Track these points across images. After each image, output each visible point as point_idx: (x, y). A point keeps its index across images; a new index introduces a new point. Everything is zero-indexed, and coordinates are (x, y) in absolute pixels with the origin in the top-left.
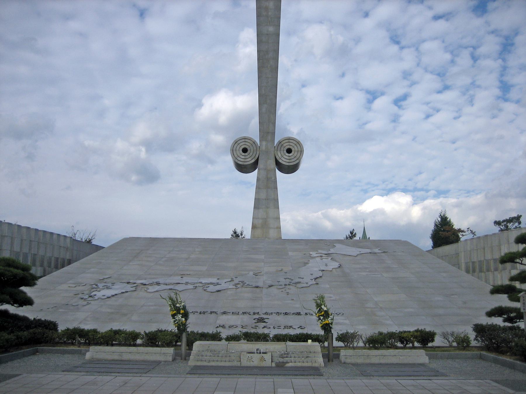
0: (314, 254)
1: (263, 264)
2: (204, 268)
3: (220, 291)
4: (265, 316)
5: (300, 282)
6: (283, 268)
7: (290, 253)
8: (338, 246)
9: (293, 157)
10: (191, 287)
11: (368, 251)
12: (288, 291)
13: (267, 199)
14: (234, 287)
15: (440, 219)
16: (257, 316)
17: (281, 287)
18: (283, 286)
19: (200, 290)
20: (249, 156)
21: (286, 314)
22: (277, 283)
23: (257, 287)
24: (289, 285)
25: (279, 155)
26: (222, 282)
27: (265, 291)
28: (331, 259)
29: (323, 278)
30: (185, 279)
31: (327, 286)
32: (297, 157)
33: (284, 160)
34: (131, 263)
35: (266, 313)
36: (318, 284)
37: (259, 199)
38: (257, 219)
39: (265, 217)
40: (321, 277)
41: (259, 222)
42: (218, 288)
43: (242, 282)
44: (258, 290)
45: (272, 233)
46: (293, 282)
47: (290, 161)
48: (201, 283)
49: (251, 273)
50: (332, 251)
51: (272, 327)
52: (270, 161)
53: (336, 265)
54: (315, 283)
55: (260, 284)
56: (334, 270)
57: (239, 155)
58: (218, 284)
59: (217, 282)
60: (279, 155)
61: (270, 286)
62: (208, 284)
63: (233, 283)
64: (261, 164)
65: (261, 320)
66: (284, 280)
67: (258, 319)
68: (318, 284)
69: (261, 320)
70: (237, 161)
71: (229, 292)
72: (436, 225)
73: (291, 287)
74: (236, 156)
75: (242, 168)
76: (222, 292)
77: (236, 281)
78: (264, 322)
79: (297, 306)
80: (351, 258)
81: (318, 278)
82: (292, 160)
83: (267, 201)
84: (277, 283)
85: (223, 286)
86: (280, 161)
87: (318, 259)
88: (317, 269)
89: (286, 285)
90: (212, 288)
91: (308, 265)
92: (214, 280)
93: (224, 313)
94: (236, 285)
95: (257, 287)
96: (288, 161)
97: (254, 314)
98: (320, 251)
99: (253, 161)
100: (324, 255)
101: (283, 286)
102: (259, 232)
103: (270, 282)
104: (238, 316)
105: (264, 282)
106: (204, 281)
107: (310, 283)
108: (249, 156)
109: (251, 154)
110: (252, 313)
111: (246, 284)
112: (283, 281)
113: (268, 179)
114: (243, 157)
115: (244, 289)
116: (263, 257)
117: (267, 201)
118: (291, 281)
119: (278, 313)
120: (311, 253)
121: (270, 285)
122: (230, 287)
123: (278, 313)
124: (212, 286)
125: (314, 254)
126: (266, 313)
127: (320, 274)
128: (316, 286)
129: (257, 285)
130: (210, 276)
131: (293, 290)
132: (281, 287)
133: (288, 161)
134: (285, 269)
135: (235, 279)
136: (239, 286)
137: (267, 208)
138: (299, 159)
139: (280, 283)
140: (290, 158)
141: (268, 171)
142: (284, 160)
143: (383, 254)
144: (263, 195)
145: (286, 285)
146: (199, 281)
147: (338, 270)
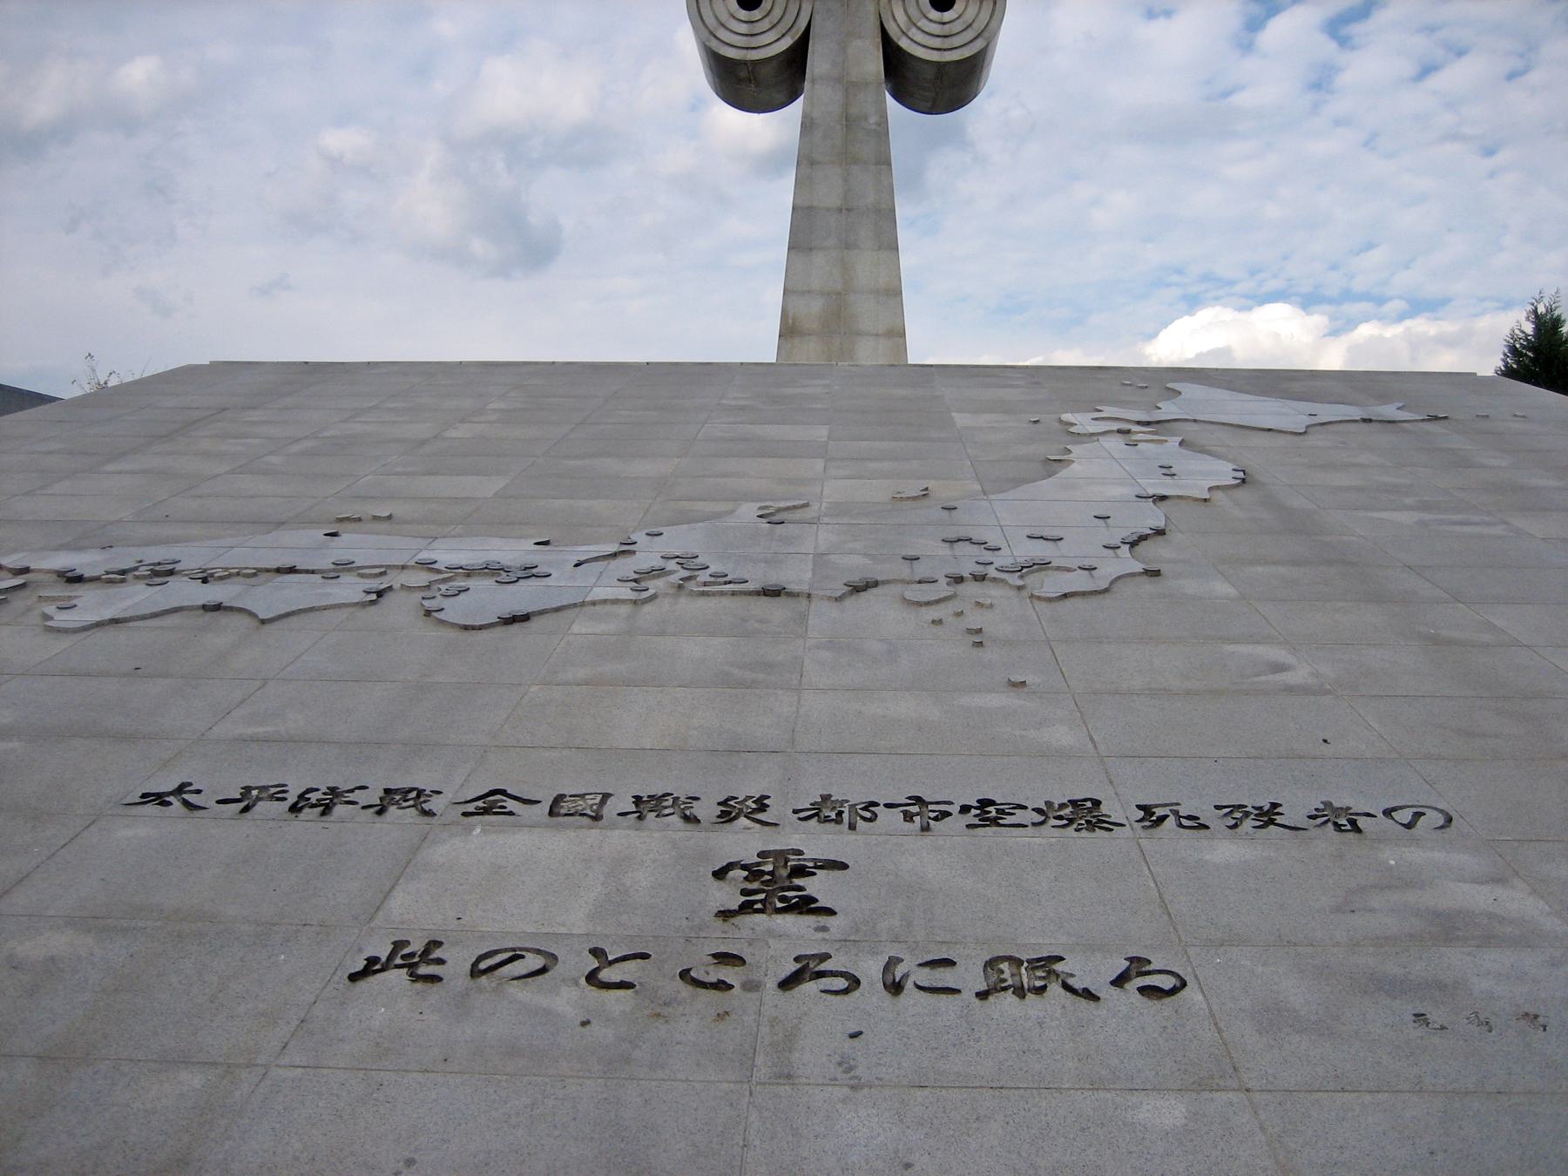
0: (1083, 422)
1: (819, 464)
2: (487, 487)
3: (526, 618)
4: (815, 842)
5: (1044, 565)
6: (931, 484)
7: (961, 420)
8: (1190, 390)
9: (957, 27)
10: (350, 589)
11: (1356, 413)
12: (974, 619)
13: (846, 209)
14: (625, 592)
15: (1529, 328)
16: (744, 842)
17: (928, 593)
18: (943, 589)
19: (400, 609)
20: (766, 24)
21: (987, 813)
22: (904, 571)
23: (773, 593)
24: (980, 578)
25: (901, 17)
26: (558, 562)
27: (823, 617)
28: (1181, 444)
29: (1175, 537)
30: (357, 546)
31: (1222, 588)
32: (978, 26)
33: (920, 37)
34: (110, 467)
35: (821, 811)
36: (1156, 573)
37: (810, 208)
38: (803, 293)
39: (839, 287)
40: (1160, 532)
41: (811, 309)
42: (521, 597)
43: (682, 561)
44: (776, 611)
45: (869, 354)
46: (1000, 560)
47: (947, 43)
48: (428, 566)
49: (749, 511)
50: (1168, 410)
51: (870, 970)
52: (858, 43)
53: (1224, 472)
54: (1138, 567)
55: (795, 575)
56: (1219, 495)
57: (724, 17)
58: (529, 572)
59: (530, 560)
60: (901, 17)
61: (857, 589)
62: (469, 573)
63: (627, 566)
64: (817, 62)
65: (778, 886)
66: (944, 550)
67: (753, 872)
68: (1156, 573)
69: (778, 886)
70: (714, 44)
71: (583, 626)
72: (1513, 350)
73: (992, 593)
74: (711, 21)
75: (741, 82)
76: (534, 624)
77: (648, 556)
78: (806, 905)
79: (1062, 735)
80: (1281, 441)
81: (1143, 538)
82: (956, 41)
83: (844, 225)
84: (904, 571)
85: (562, 583)
86: (904, 43)
87: (1115, 444)
88: (1127, 491)
89: (959, 580)
90: (486, 599)
91: (1064, 473)
92: (513, 551)
93: (490, 804)
94: (639, 579)
95: (773, 593)
96: (937, 43)
97: (728, 813)
98: (1108, 411)
99: (787, 43)
100: (1135, 428)
101: (943, 589)
102: (809, 351)
103: (857, 565)
104: (593, 835)
105: (820, 558)
106: (447, 555)
107: (1110, 568)
108: (766, 24)
109: (777, 13)
110: (707, 810)
111: (704, 576)
112: (938, 559)
113: (850, 122)
114: (743, 28)
115: (688, 607)
116: (822, 432)
117: (844, 225)
118: (988, 556)
119: (921, 811)
120: (1067, 417)
121: (856, 578)
122: (600, 593)
123: (921, 811)
124: (489, 582)
125: (1083, 422)
126: (821, 811)
127: (1154, 517)
128: (1148, 586)
129: (774, 578)
130: (503, 526)
131: (1003, 610)
132: (928, 593)
133: (937, 43)
134: (943, 491)
135: (640, 537)
136: (655, 586)
137: (848, 246)
138: (988, 33)
139: (921, 570)
140: (946, 29)
141: (849, 86)
142: (920, 37)
143: (1429, 427)
144: (828, 194)
145: (959, 580)
146: (425, 556)
147: (1241, 494)
